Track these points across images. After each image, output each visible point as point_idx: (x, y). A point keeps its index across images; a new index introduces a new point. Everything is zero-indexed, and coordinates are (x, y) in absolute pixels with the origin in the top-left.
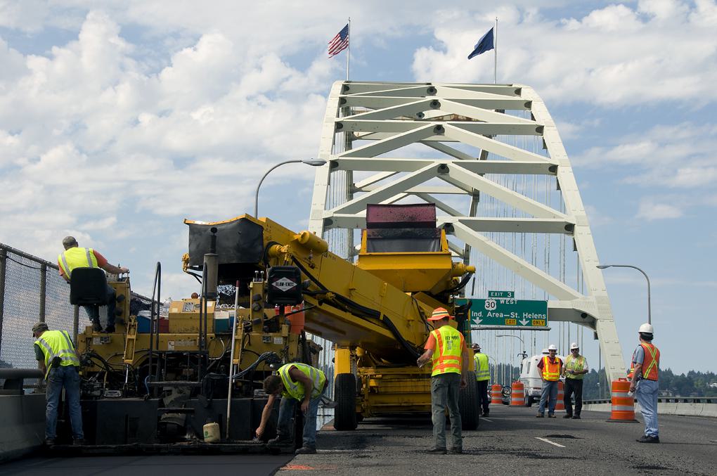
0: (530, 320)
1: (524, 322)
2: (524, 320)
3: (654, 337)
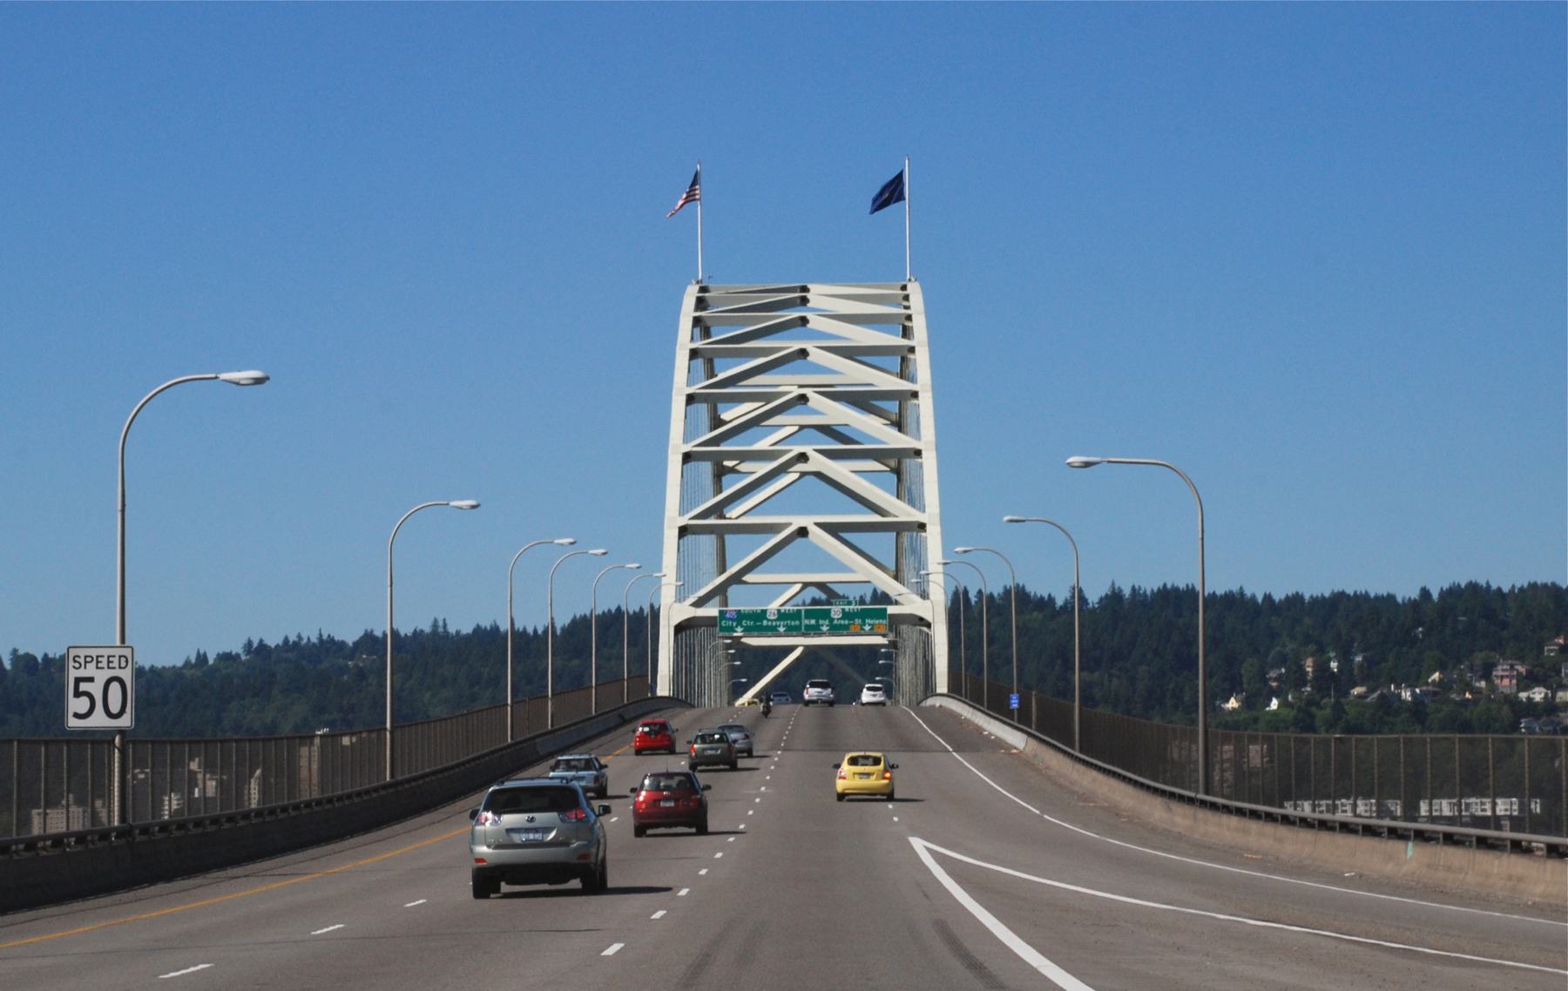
1: (867, 628)
3: (633, 831)
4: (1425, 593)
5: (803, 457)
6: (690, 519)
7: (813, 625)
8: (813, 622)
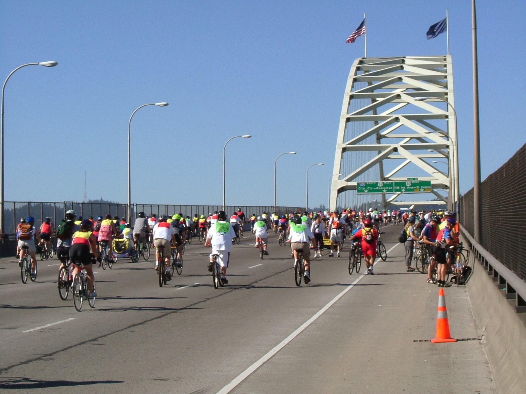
1: (422, 190)
5: (397, 119)
6: (347, 145)
7: (398, 189)
8: (398, 188)
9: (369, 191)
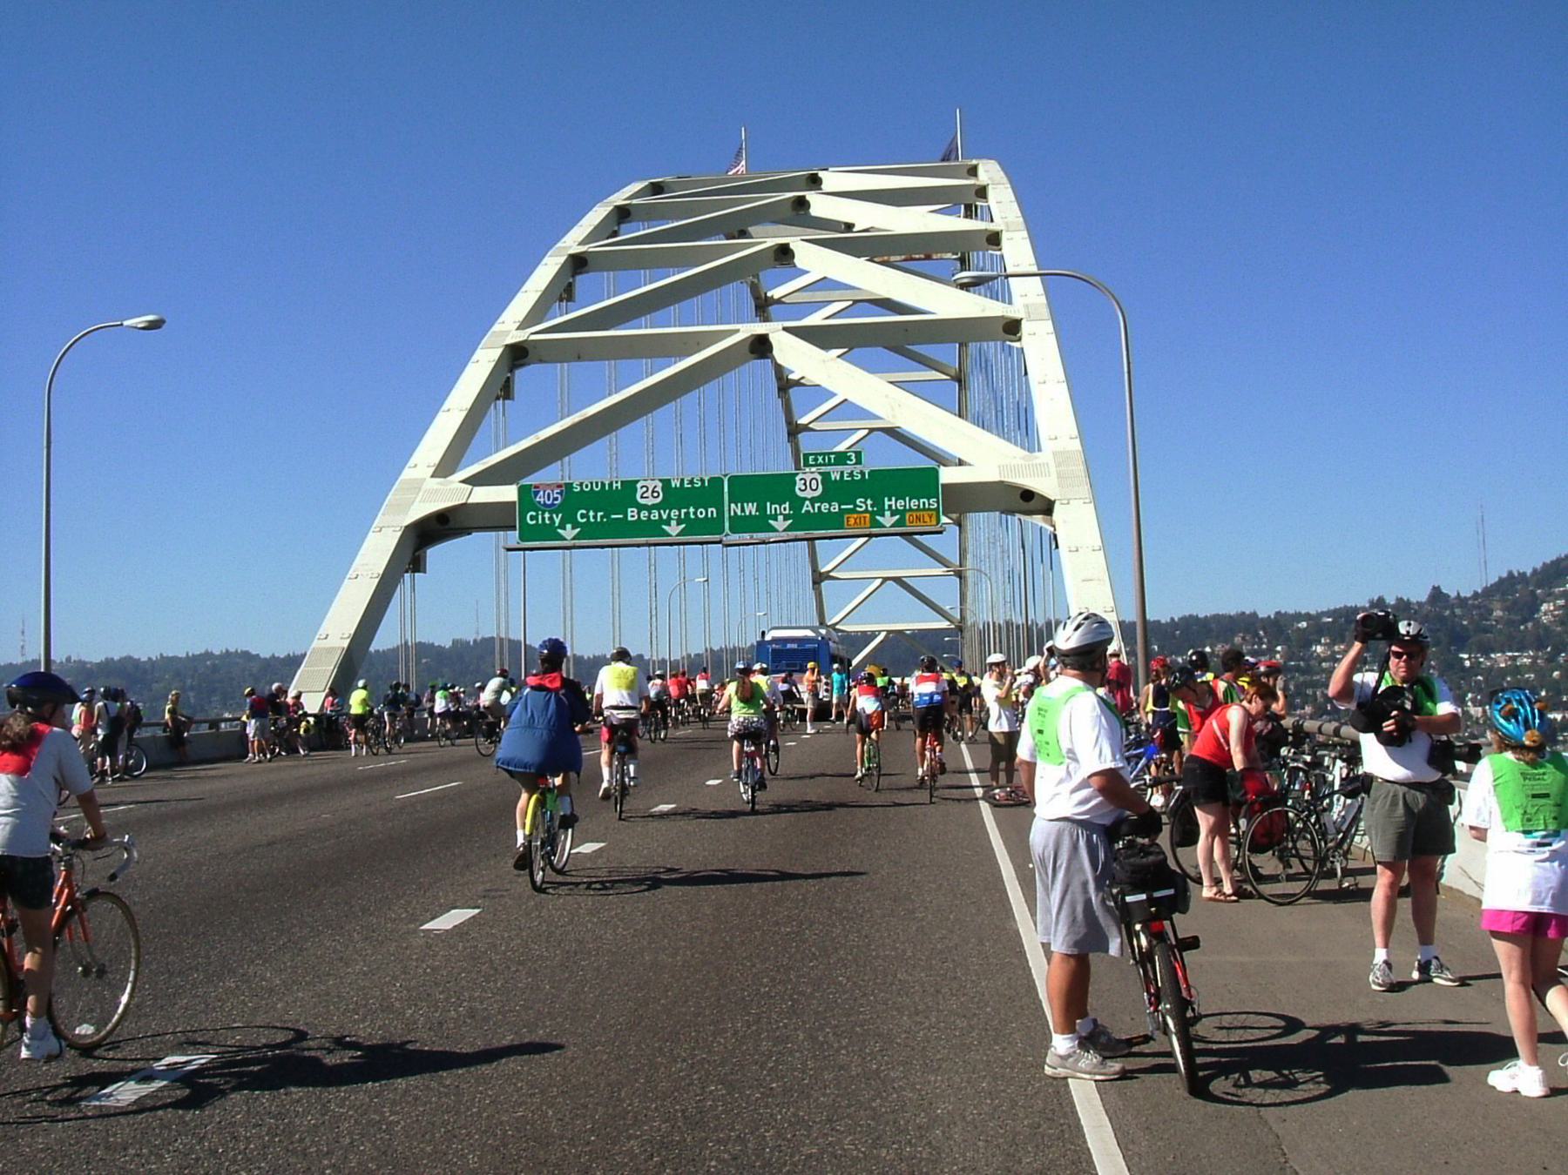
0: (902, 513)
1: (888, 520)
2: (888, 513)
4: (1172, 619)
8: (751, 508)
9: (588, 531)
